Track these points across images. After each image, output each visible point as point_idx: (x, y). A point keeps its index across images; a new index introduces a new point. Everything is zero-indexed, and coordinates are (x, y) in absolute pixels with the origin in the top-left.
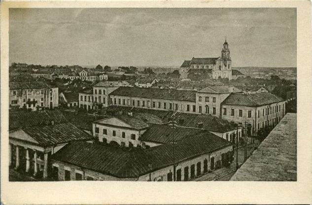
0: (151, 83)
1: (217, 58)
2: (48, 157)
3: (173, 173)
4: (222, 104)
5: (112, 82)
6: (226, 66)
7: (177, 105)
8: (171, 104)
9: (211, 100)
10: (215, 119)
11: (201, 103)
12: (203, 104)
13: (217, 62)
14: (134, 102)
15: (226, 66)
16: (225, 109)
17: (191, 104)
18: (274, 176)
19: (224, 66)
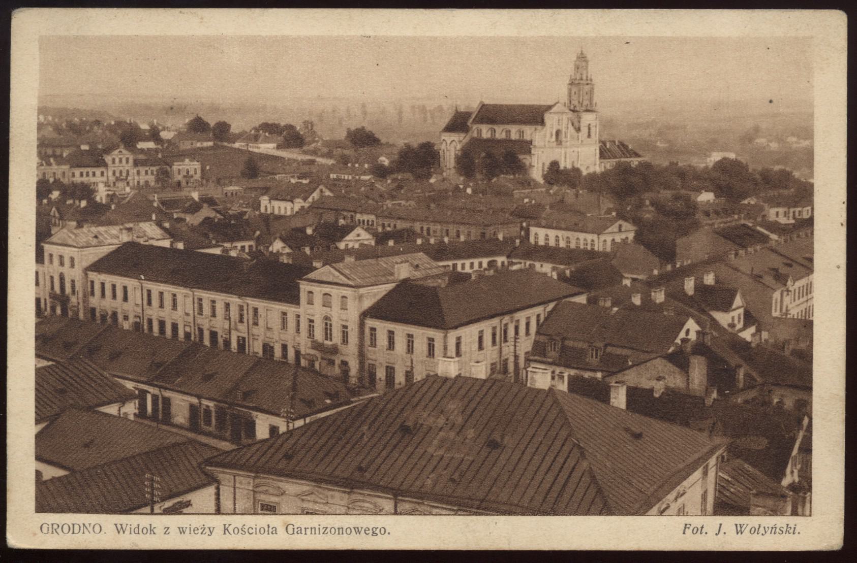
0: (305, 199)
1: (549, 107)
2: (348, 234)
3: (545, 359)
4: (364, 315)
5: (102, 229)
6: (578, 130)
7: (256, 310)
8: (241, 308)
9: (336, 302)
10: (572, 251)
11: (310, 310)
12: (317, 311)
13: (549, 118)
14: (149, 295)
15: (578, 130)
16: (373, 329)
17: (291, 310)
18: (519, 510)
19: (571, 129)
